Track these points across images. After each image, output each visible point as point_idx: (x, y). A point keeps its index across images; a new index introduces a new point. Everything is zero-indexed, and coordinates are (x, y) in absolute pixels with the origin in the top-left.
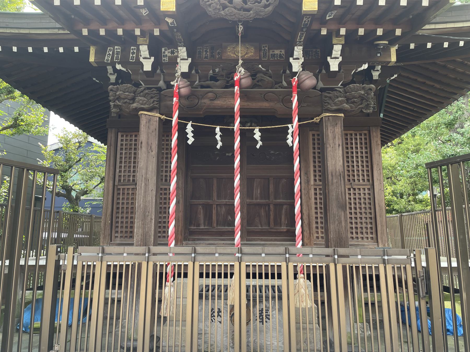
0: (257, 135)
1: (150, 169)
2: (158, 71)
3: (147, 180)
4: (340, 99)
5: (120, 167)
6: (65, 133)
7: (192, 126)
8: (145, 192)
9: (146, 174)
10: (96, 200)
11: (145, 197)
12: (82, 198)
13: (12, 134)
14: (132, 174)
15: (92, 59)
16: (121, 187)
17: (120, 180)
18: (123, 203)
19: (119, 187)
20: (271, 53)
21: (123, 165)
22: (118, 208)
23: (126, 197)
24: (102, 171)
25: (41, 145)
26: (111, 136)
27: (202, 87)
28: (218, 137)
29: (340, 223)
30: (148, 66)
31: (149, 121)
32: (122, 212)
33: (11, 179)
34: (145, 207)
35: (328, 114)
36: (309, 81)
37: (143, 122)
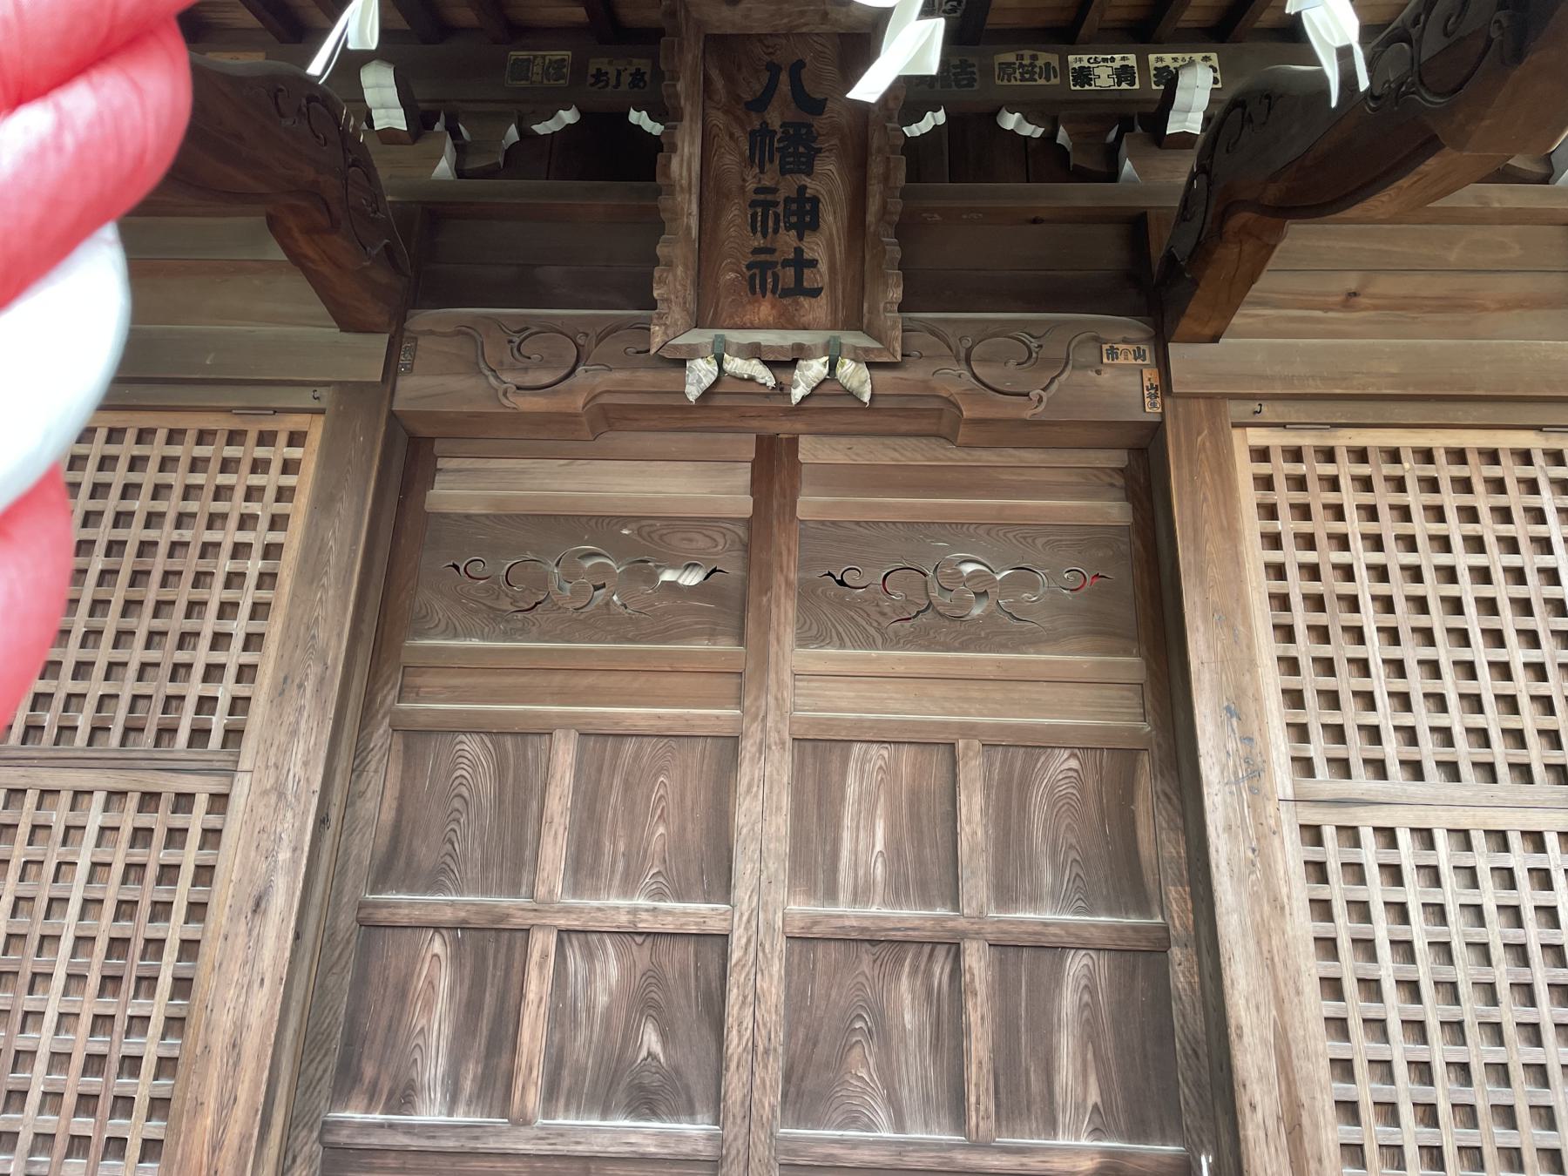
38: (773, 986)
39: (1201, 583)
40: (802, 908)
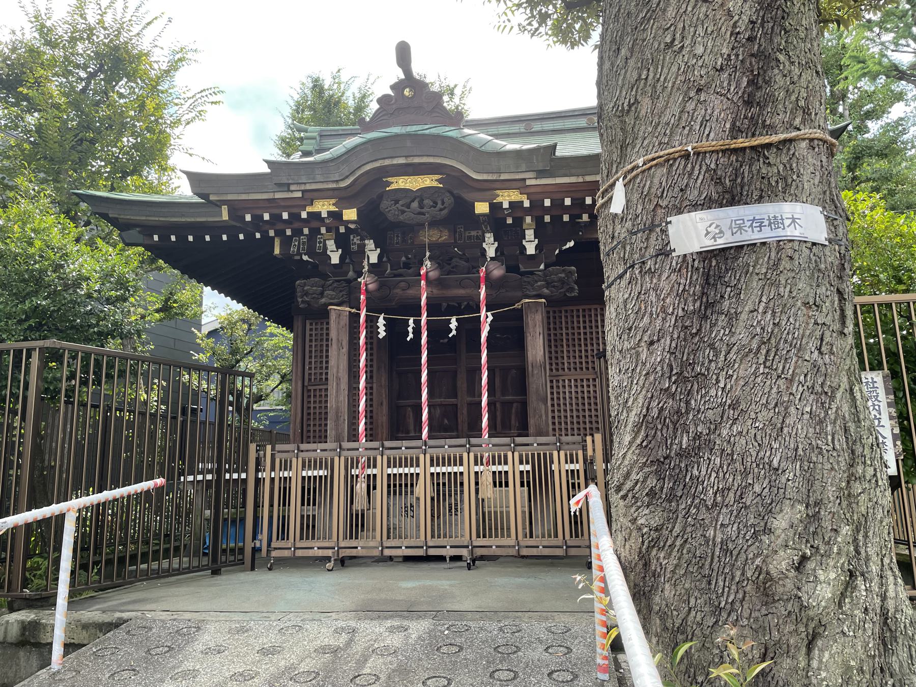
0: (454, 324)
1: (341, 367)
2: (347, 261)
3: (338, 379)
4: (539, 283)
5: (310, 363)
6: (229, 312)
7: (384, 318)
8: (337, 392)
9: (338, 372)
10: (273, 410)
11: (337, 396)
12: (255, 407)
13: (160, 320)
14: (324, 371)
15: (277, 251)
16: (312, 388)
17: (310, 380)
18: (315, 408)
19: (309, 388)
20: (467, 234)
21: (313, 360)
22: (309, 414)
23: (318, 399)
24: (285, 365)
25: (196, 331)
26: (298, 324)
27: (395, 276)
28: (410, 329)
29: (541, 417)
30: (335, 259)
31: (339, 314)
32: (315, 419)
33: (168, 384)
34: (338, 408)
35: (527, 300)
36: (498, 272)
37: (333, 317)
38: (465, 411)
39: (884, 614)
40: (470, 399)
